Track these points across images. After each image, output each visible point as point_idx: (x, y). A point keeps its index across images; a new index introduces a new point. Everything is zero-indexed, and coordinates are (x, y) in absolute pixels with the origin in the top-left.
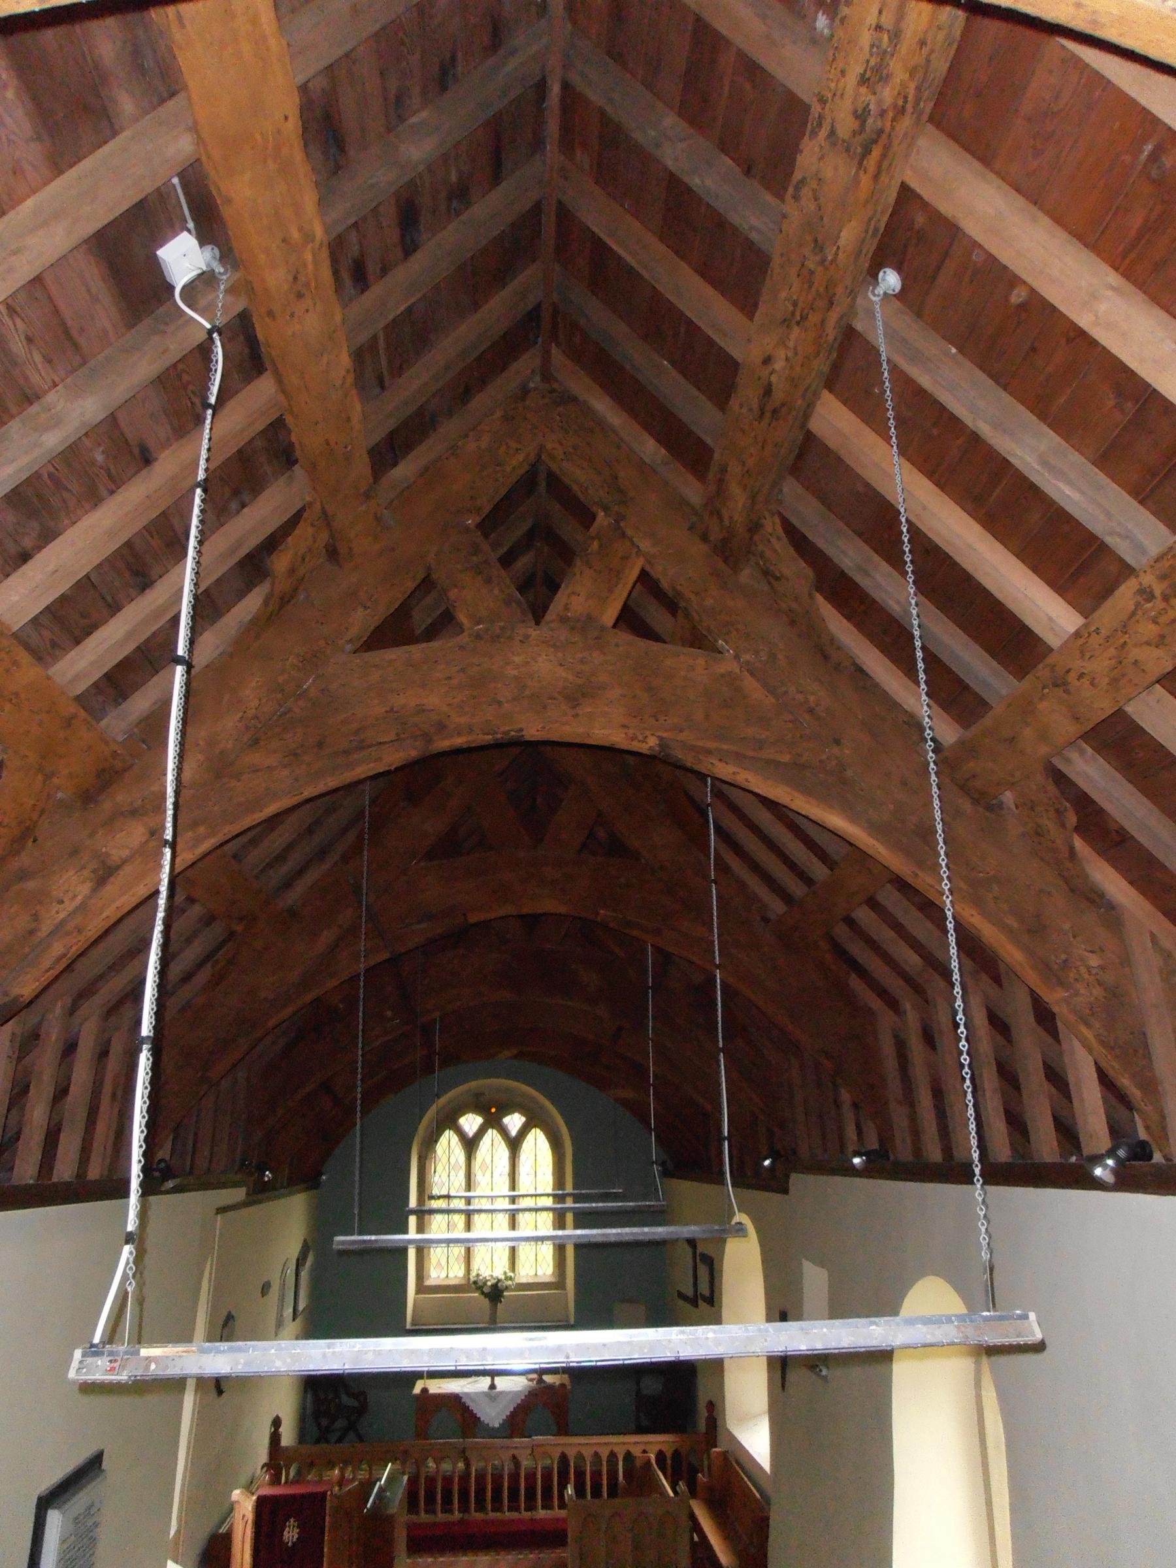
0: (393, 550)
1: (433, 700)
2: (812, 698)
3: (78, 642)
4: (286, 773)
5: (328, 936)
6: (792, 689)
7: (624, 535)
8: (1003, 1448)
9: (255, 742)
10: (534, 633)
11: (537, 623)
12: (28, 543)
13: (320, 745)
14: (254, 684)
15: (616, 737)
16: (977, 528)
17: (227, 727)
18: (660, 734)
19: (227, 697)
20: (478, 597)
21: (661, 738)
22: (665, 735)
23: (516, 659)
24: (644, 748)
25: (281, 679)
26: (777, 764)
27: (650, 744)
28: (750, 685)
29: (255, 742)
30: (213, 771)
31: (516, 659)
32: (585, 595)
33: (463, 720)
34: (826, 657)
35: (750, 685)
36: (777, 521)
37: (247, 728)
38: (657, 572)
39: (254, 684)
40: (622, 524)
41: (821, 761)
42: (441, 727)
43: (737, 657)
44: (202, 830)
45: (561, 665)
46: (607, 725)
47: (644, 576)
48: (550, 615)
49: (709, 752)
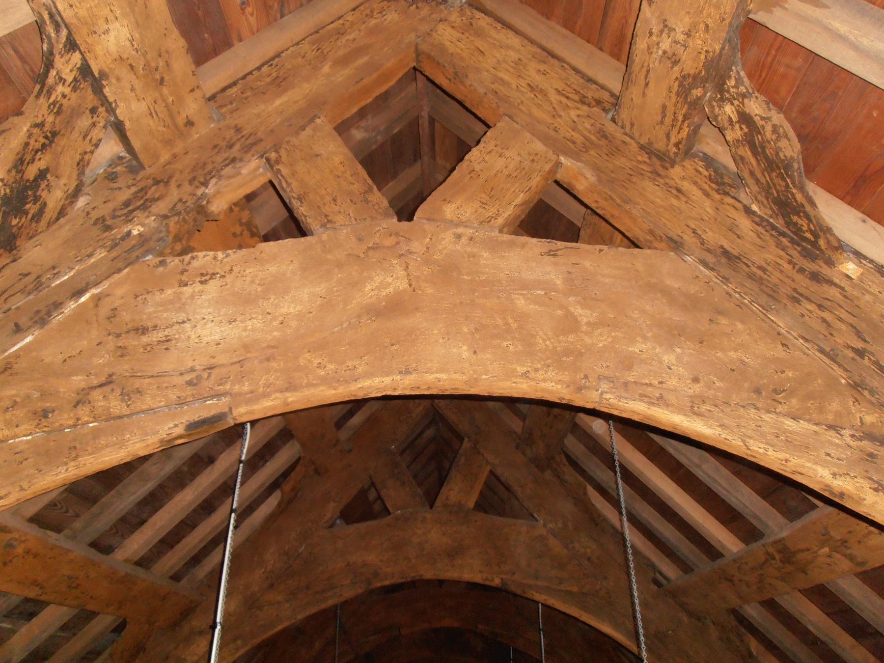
0: (350, 466)
1: (372, 558)
2: (589, 551)
3: (172, 547)
4: (288, 605)
5: (318, 645)
6: (577, 545)
7: (479, 453)
8: (780, 472)
9: (272, 586)
10: (428, 516)
11: (431, 507)
12: (145, 516)
13: (307, 588)
14: (271, 551)
15: (478, 578)
16: (674, 485)
17: (257, 577)
18: (501, 576)
19: (256, 559)
20: (397, 495)
21: (502, 579)
22: (504, 577)
23: (419, 532)
24: (493, 584)
25: (287, 548)
26: (570, 593)
27: (497, 582)
28: (553, 542)
29: (272, 586)
30: (248, 605)
31: (419, 532)
32: (459, 491)
33: (389, 570)
34: (597, 525)
35: (553, 542)
36: (563, 456)
37: (267, 578)
38: (498, 471)
39: (271, 551)
40: (478, 446)
41: (596, 591)
42: (376, 574)
43: (545, 525)
44: (239, 642)
45: (444, 534)
46: (471, 570)
47: (491, 472)
48: (438, 503)
49: (530, 587)
